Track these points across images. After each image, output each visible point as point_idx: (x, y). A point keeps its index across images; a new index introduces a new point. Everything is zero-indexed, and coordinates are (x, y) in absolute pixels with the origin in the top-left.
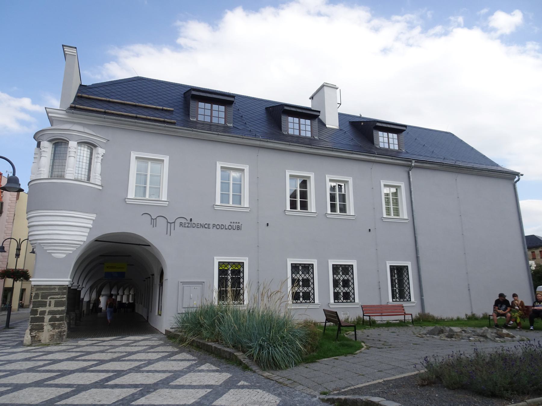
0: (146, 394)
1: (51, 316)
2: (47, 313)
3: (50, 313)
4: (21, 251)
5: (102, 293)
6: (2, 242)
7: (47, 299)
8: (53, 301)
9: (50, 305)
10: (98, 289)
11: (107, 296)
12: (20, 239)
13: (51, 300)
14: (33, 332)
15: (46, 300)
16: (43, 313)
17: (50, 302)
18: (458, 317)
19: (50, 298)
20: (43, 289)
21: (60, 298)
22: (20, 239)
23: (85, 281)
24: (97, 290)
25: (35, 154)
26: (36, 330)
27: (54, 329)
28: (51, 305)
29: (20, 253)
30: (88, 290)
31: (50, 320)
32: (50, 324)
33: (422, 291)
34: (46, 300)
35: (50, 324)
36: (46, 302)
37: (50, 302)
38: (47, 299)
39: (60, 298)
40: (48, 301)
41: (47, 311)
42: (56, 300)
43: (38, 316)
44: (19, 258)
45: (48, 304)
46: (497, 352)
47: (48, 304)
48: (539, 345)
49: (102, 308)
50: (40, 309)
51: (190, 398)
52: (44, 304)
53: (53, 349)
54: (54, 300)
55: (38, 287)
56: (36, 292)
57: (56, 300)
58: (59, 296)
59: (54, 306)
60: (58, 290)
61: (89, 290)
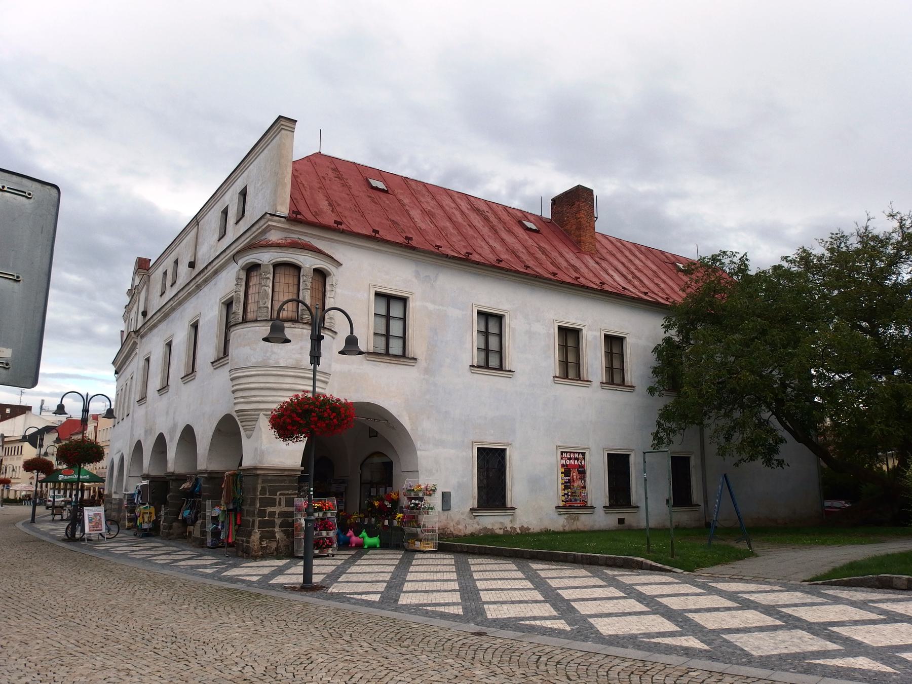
2: (277, 516)
3: (281, 514)
8: (283, 498)
9: (280, 504)
12: (87, 395)
13: (281, 497)
14: (263, 541)
15: (275, 497)
16: (272, 514)
17: (280, 499)
18: (330, 274)
19: (280, 495)
20: (270, 481)
22: (87, 395)
25: (375, 334)
26: (267, 538)
32: (282, 531)
33: (363, 238)
34: (275, 497)
36: (275, 499)
37: (280, 499)
40: (277, 497)
41: (277, 512)
43: (267, 518)
45: (277, 503)
46: (432, 508)
47: (277, 503)
50: (269, 509)
51: (591, 660)
52: (272, 503)
53: (864, 595)
54: (285, 496)
55: (265, 478)
56: (263, 485)
58: (290, 492)
60: (289, 482)
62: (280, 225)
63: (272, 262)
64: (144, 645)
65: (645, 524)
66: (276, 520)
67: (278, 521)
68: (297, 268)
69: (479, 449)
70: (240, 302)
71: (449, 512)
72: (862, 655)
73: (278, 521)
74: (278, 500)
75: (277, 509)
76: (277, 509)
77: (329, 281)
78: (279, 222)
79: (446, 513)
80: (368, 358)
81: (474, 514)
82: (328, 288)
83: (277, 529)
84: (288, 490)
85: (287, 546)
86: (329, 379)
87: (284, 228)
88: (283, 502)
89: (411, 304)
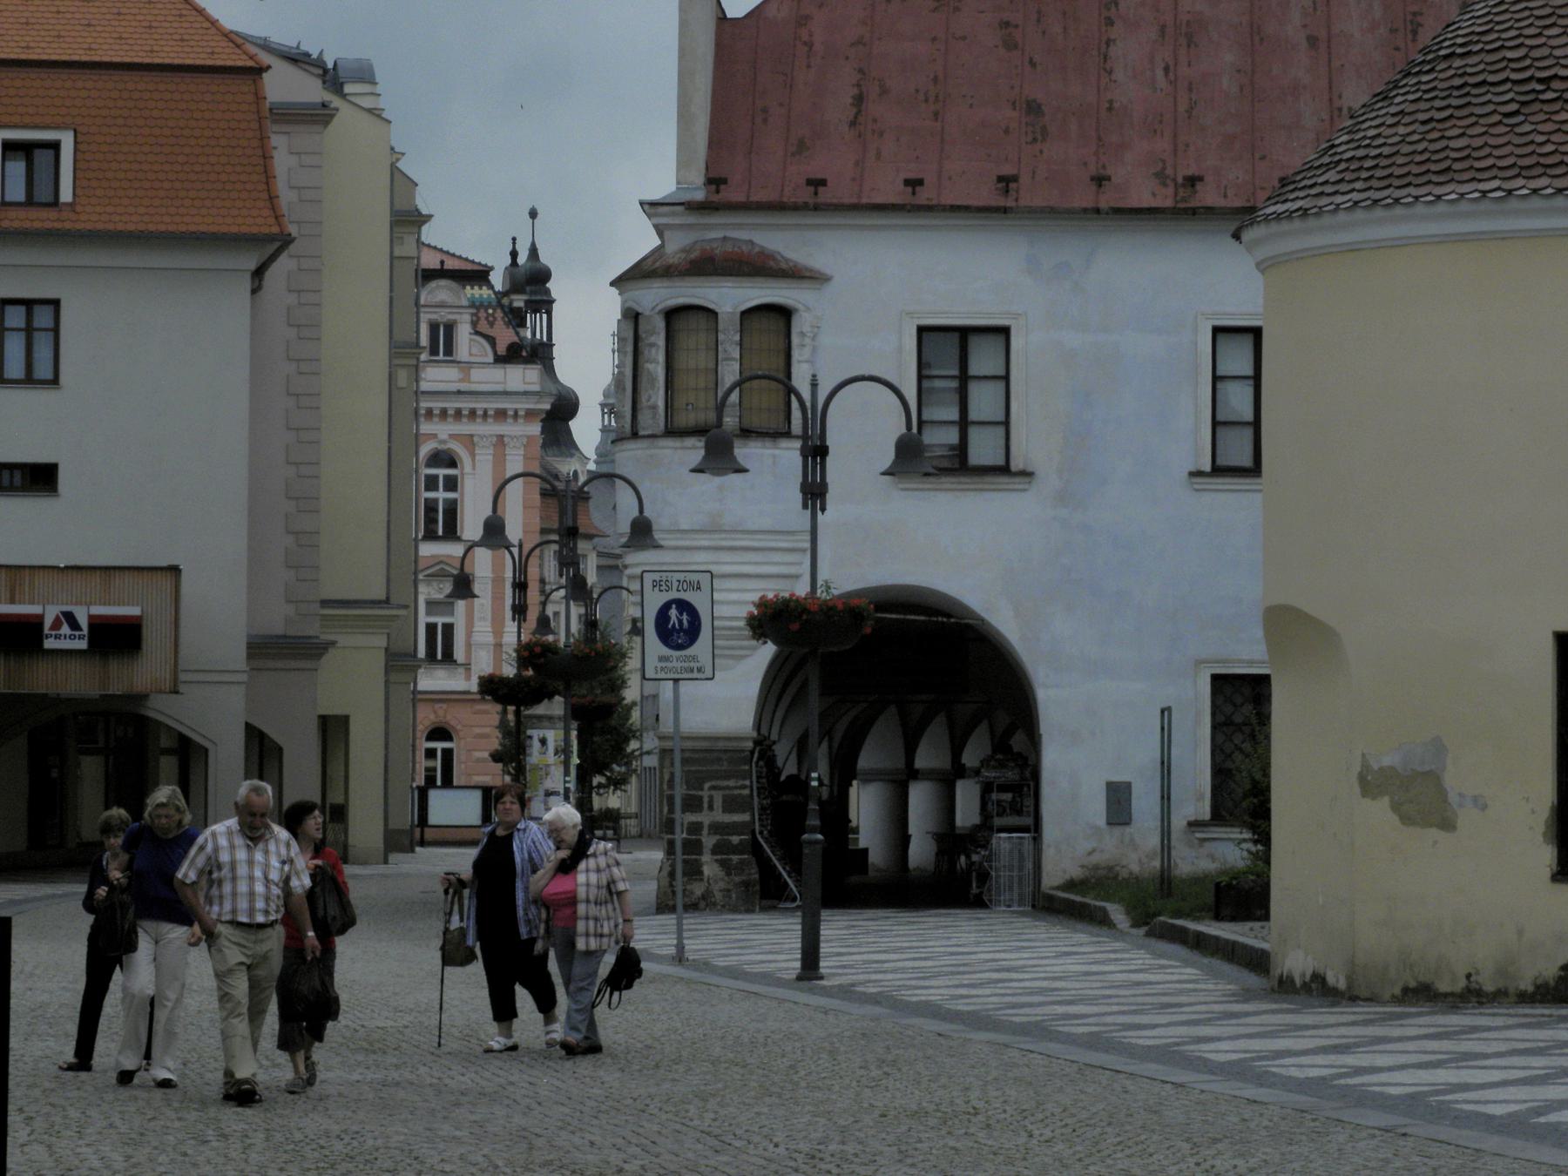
0: (323, 983)
1: (718, 837)
2: (705, 831)
3: (716, 828)
4: (829, 459)
5: (865, 761)
6: (866, 373)
7: (702, 789)
9: (711, 808)
10: (836, 745)
11: (893, 781)
13: (713, 792)
15: (700, 793)
18: (796, 310)
21: (736, 788)
23: (778, 709)
24: (830, 747)
27: (728, 874)
28: (715, 807)
29: (829, 479)
30: (790, 753)
31: (716, 850)
32: (716, 860)
34: (700, 793)
35: (716, 860)
36: (701, 798)
37: (711, 798)
38: (702, 789)
39: (736, 788)
40: (705, 794)
42: (727, 792)
44: (823, 509)
45: (706, 805)
47: (706, 805)
48: (495, 775)
49: (865, 851)
57: (727, 792)
58: (731, 783)
59: (721, 810)
61: (795, 749)
62: (677, 221)
63: (660, 307)
64: (620, 1141)
65: (184, 680)
66: (704, 840)
67: (709, 841)
68: (711, 314)
69: (1216, 678)
70: (624, 389)
71: (1128, 830)
72: (582, 816)
73: (709, 841)
74: (706, 800)
75: (705, 818)
76: (705, 818)
77: (797, 325)
78: (674, 214)
79: (1117, 831)
80: (901, 486)
81: (1198, 835)
82: (795, 340)
83: (706, 858)
84: (727, 777)
85: (729, 891)
86: (1260, 484)
87: (689, 225)
88: (718, 803)
89: (1016, 342)
